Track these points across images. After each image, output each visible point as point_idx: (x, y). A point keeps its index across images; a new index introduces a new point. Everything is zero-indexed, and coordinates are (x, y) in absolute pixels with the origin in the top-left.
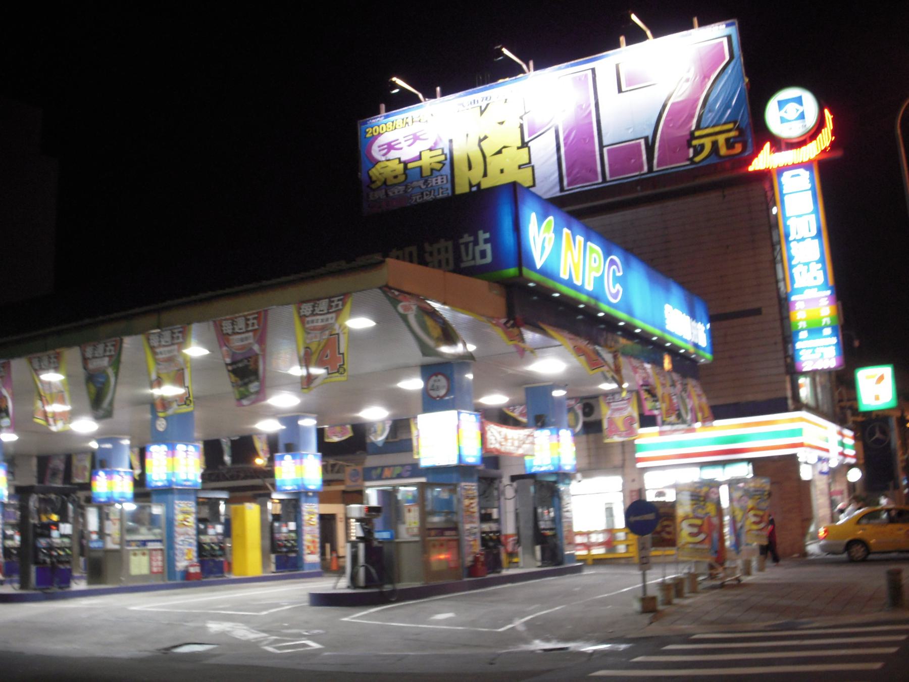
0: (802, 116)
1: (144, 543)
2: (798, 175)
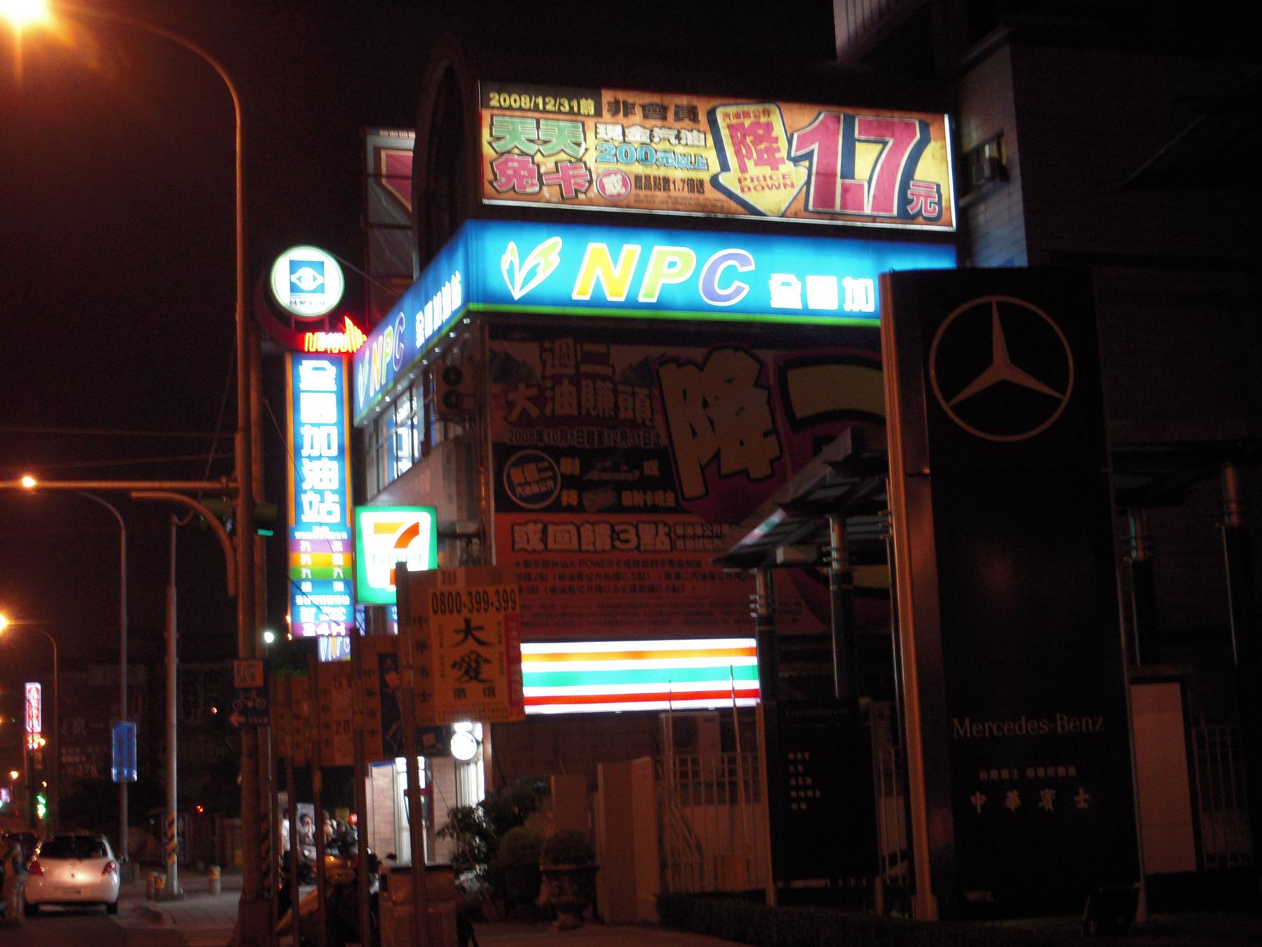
0: (321, 289)
1: (732, 772)
2: (323, 369)
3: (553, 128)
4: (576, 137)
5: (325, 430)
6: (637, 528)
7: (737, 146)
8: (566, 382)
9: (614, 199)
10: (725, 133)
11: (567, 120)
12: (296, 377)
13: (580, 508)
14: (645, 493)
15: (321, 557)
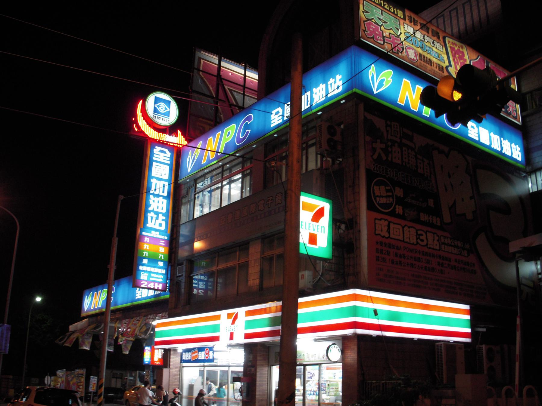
0: (168, 114)
3: (388, 18)
4: (396, 25)
5: (162, 183)
6: (426, 234)
7: (454, 56)
8: (396, 145)
9: (411, 61)
10: (449, 49)
11: (393, 16)
12: (152, 153)
13: (402, 217)
14: (429, 217)
15: (154, 247)
